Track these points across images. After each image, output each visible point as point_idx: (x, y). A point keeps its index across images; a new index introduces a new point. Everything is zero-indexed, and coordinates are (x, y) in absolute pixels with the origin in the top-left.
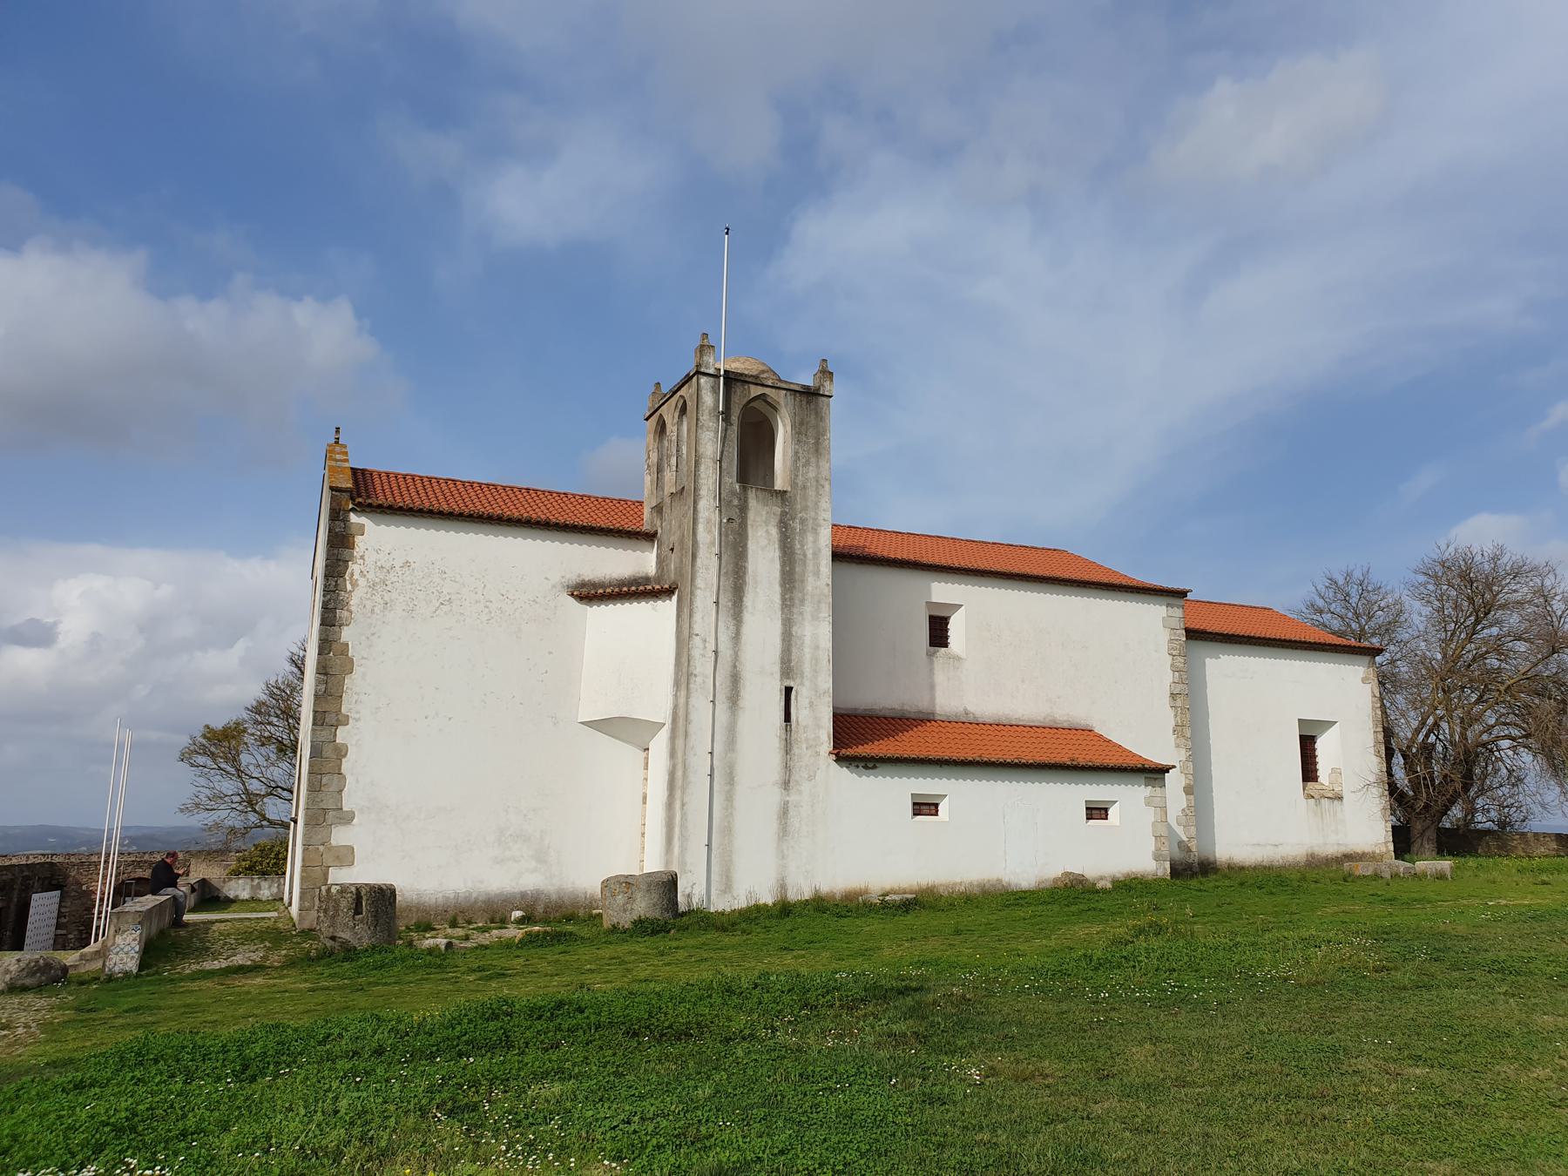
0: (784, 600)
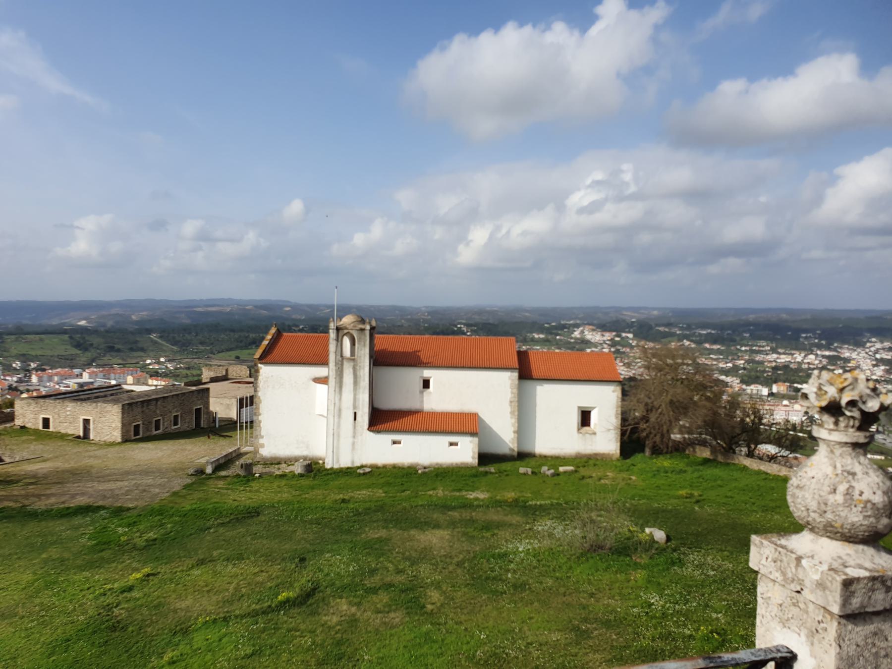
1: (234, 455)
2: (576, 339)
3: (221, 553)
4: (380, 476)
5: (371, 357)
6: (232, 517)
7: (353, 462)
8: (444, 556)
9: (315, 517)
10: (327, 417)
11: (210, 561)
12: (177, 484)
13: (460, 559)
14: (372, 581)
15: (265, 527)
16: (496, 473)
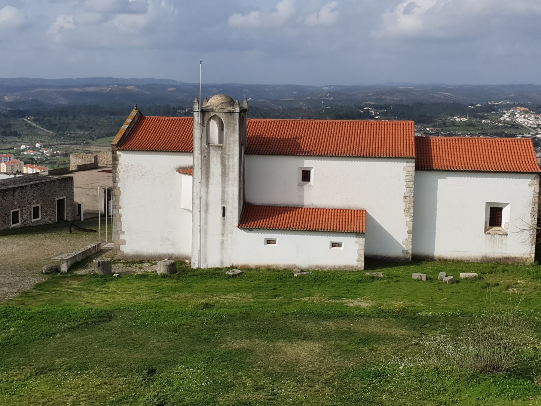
0: (222, 180)
1: (93, 252)
2: (505, 122)
3: (64, 362)
4: (251, 280)
5: (241, 144)
6: (82, 321)
7: (222, 263)
8: (312, 371)
9: (173, 323)
10: (192, 212)
11: (50, 370)
12: (29, 283)
13: (329, 377)
14: (226, 398)
15: (116, 333)
16: (384, 279)
